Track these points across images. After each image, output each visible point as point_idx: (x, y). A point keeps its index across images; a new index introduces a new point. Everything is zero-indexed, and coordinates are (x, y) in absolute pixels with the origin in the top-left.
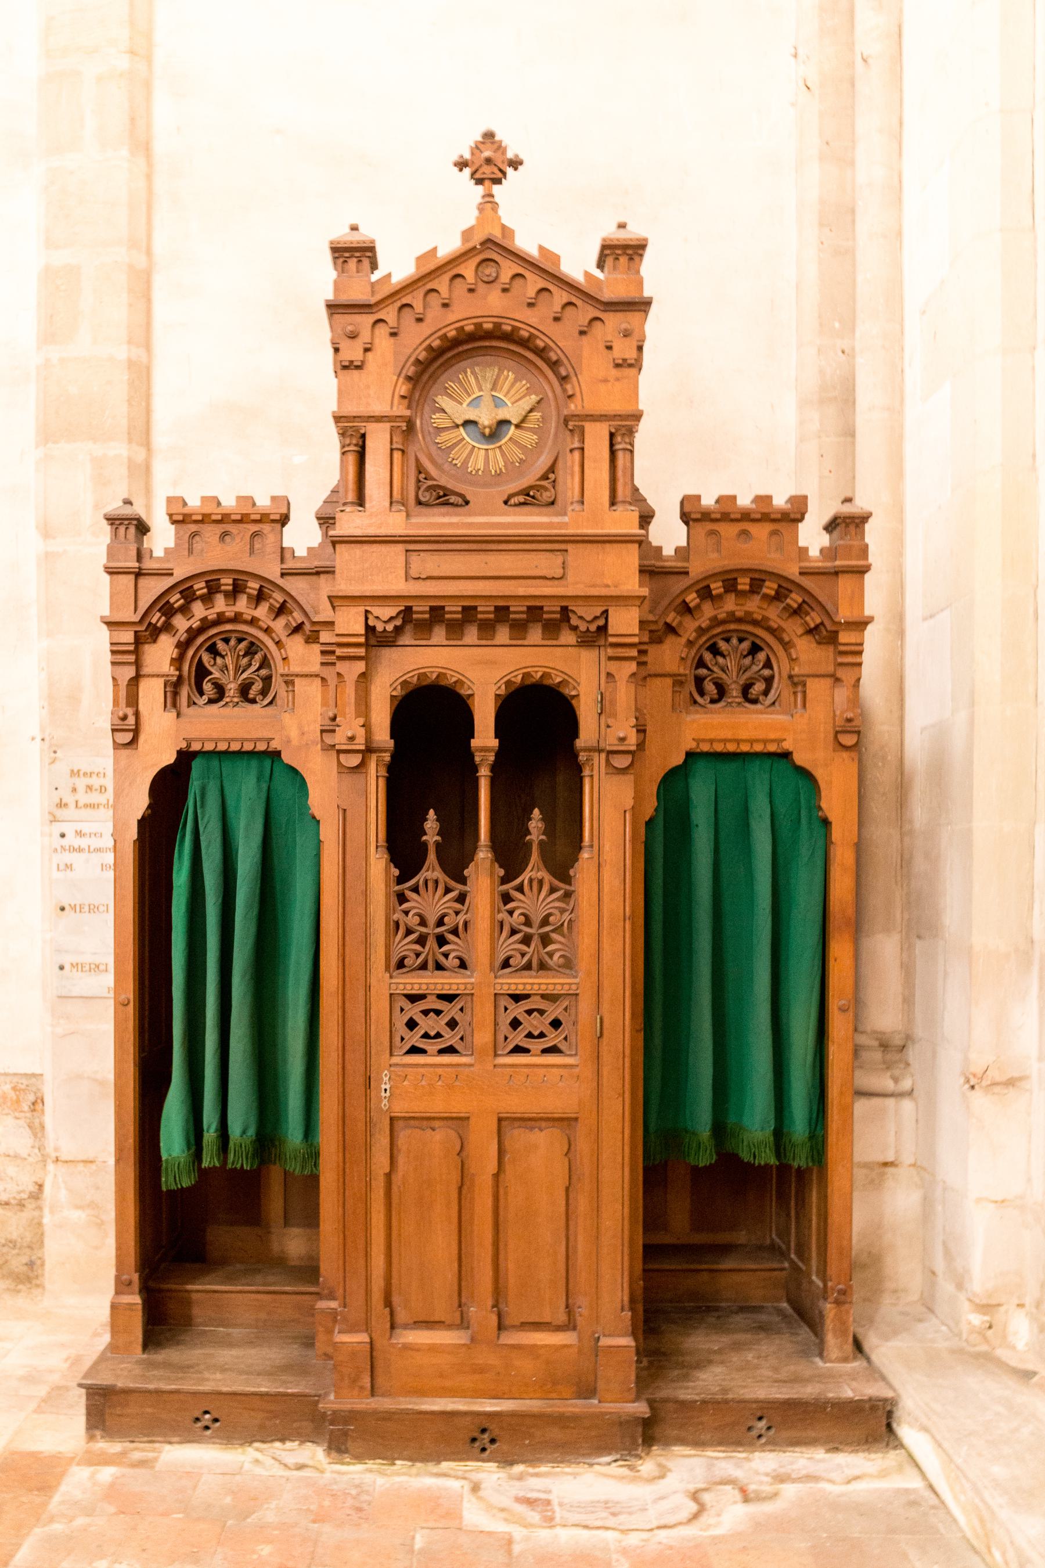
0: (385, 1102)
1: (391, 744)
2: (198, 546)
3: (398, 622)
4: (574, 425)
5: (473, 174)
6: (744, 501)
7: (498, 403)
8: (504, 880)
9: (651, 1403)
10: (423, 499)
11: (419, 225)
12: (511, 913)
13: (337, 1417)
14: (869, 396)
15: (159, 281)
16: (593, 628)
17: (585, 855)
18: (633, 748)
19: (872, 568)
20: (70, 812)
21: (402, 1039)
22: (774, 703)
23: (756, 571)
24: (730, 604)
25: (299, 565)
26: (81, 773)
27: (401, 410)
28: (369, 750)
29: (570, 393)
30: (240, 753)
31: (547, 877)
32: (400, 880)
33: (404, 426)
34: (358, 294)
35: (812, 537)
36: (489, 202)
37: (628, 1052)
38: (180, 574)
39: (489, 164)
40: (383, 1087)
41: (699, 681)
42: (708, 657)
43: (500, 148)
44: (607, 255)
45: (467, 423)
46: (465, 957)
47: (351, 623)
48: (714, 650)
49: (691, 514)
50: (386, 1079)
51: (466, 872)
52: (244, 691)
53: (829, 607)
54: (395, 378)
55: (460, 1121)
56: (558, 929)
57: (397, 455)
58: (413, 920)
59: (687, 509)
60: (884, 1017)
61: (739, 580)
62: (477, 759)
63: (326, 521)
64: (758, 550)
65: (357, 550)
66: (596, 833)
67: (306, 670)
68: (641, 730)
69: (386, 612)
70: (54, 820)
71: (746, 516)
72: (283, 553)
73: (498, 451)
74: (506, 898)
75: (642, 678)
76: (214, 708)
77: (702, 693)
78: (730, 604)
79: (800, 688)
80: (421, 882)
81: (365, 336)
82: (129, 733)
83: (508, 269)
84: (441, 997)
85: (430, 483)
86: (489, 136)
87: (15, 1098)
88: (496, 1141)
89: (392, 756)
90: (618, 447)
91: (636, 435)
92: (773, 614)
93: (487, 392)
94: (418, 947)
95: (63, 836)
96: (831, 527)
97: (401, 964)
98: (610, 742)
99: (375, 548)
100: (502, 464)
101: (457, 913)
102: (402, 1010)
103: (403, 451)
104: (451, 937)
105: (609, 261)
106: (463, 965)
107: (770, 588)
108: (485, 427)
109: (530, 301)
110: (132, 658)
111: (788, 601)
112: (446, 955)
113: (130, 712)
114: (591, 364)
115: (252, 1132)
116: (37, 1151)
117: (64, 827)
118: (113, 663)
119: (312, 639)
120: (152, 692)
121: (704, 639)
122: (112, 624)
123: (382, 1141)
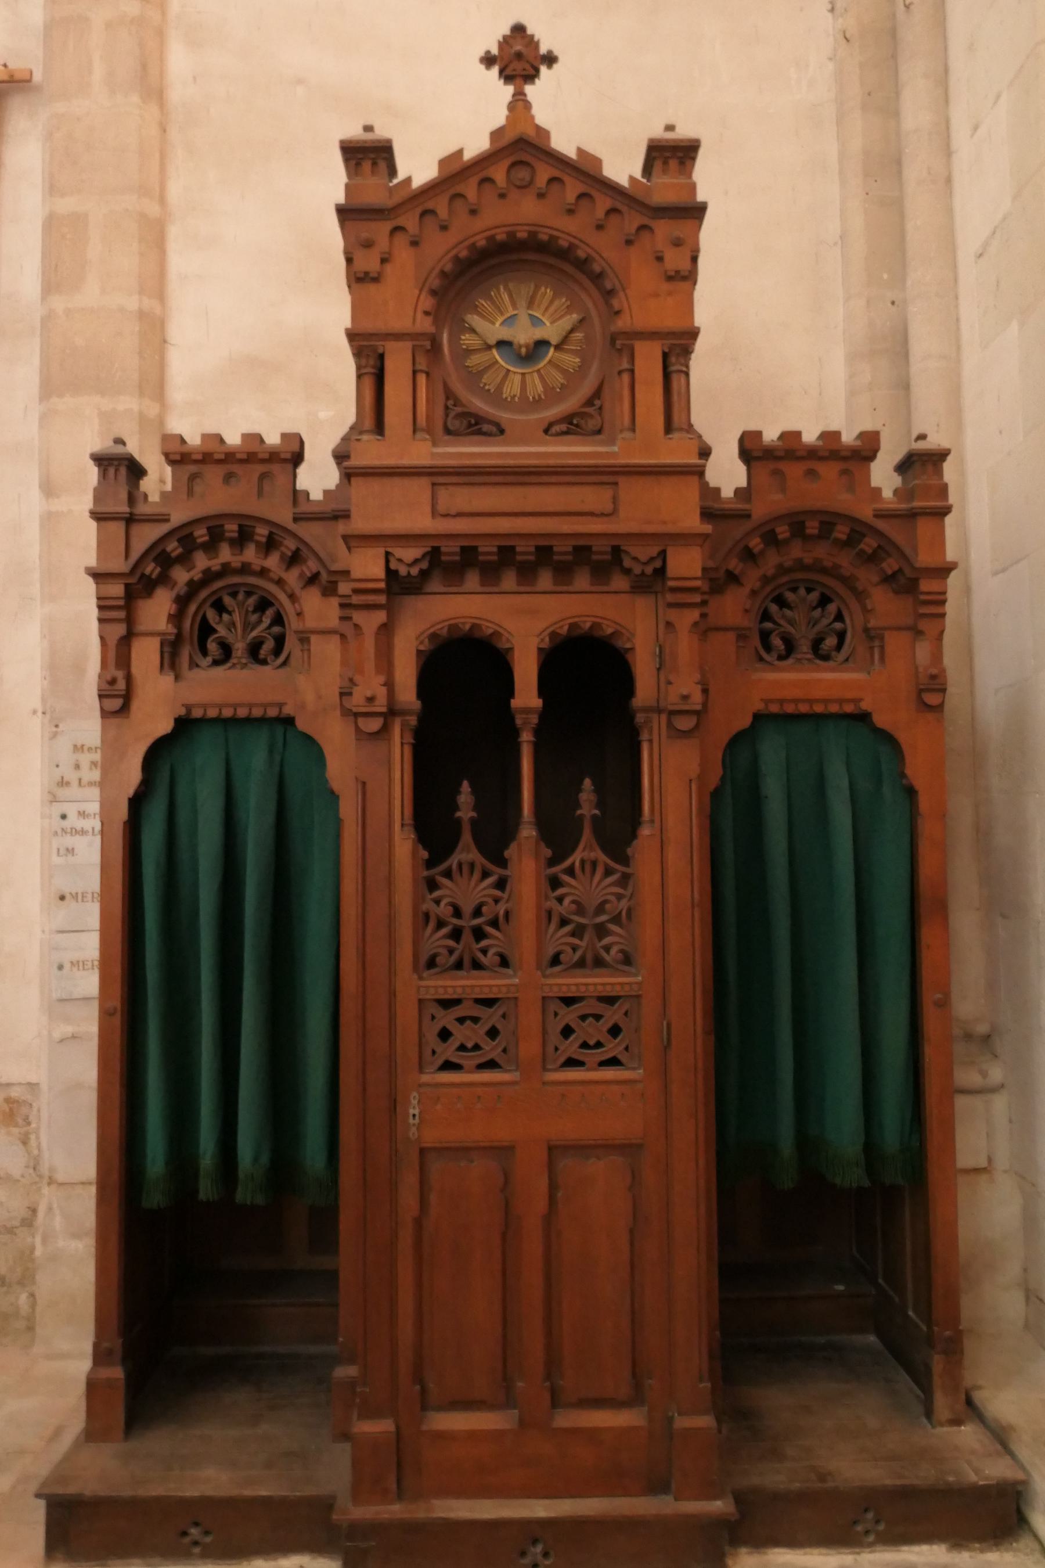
0: (414, 1129)
1: (417, 705)
2: (198, 488)
3: (425, 565)
4: (621, 344)
5: (501, 72)
6: (810, 436)
7: (535, 321)
8: (552, 862)
9: (739, 1498)
10: (451, 428)
11: (446, 121)
12: (560, 900)
13: (357, 1530)
14: (924, 343)
15: (174, 232)
16: (649, 570)
17: (645, 831)
18: (699, 707)
19: (954, 509)
20: (74, 791)
21: (434, 1052)
22: (847, 660)
23: (827, 512)
24: (796, 551)
25: (316, 509)
26: (85, 748)
27: (425, 325)
28: (392, 712)
29: (616, 308)
30: (248, 720)
31: (603, 858)
32: (430, 864)
33: (428, 344)
34: (374, 195)
35: (883, 476)
36: (519, 104)
37: (700, 1065)
38: (178, 518)
39: (519, 59)
40: (412, 1111)
41: (765, 637)
42: (774, 608)
43: (532, 43)
44: (654, 158)
45: (501, 344)
46: (506, 952)
47: (369, 566)
48: (781, 602)
49: (751, 450)
50: (415, 1102)
51: (506, 854)
52: (254, 651)
53: (908, 551)
54: (417, 292)
55: (503, 1152)
56: (616, 920)
57: (422, 379)
58: (444, 910)
59: (748, 445)
60: (968, 1002)
61: (807, 524)
62: (518, 722)
63: (340, 456)
64: (827, 492)
65: (376, 485)
66: (657, 806)
67: (323, 625)
68: (705, 691)
69: (409, 553)
70: (54, 799)
71: (812, 453)
72: (297, 496)
73: (535, 375)
74: (555, 883)
75: (704, 630)
76: (219, 671)
77: (768, 647)
78: (796, 551)
79: (877, 643)
80: (454, 867)
81: (383, 243)
82: (118, 698)
83: (544, 173)
84: (479, 1001)
85: (459, 409)
86: (519, 29)
87: (8, 1110)
88: (546, 1176)
89: (420, 720)
90: (673, 368)
91: (693, 356)
92: (845, 561)
93: (520, 316)
94: (451, 943)
95: (64, 817)
96: (904, 466)
97: (431, 963)
98: (672, 699)
99: (397, 480)
100: (540, 388)
101: (497, 901)
102: (433, 1017)
103: (428, 374)
104: (490, 930)
105: (658, 165)
106: (504, 962)
107: (841, 532)
108: (520, 346)
109: (569, 207)
110: (122, 614)
111: (862, 546)
112: (484, 951)
113: (120, 675)
114: (639, 277)
115: (265, 1159)
116: (31, 1171)
117: (66, 808)
118: (101, 620)
119: (329, 590)
120: (146, 654)
121: (769, 589)
122: (98, 576)
123: (410, 1179)
